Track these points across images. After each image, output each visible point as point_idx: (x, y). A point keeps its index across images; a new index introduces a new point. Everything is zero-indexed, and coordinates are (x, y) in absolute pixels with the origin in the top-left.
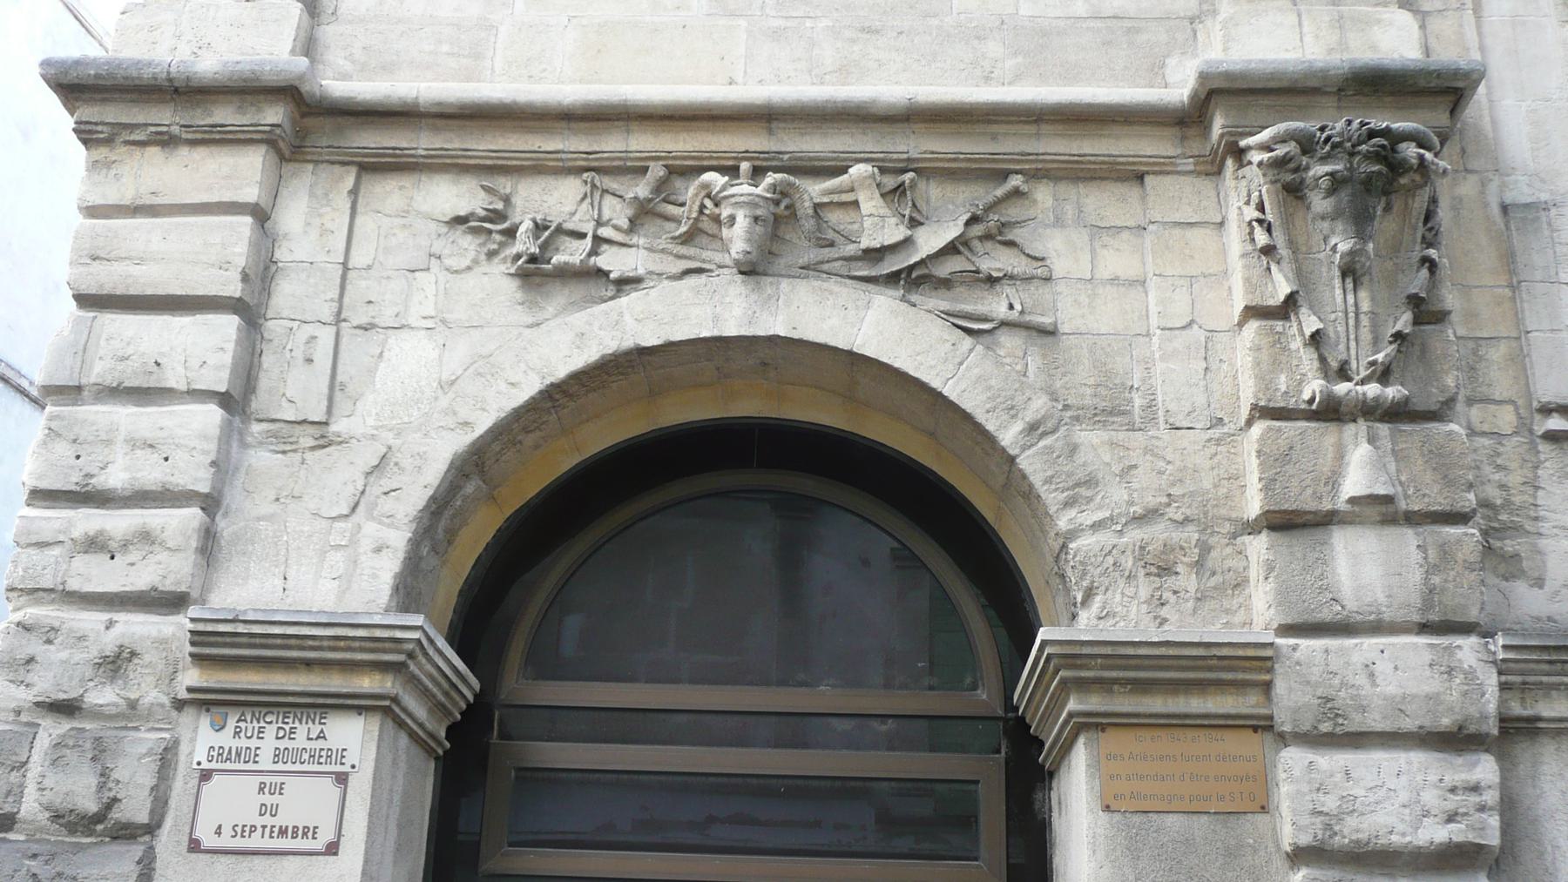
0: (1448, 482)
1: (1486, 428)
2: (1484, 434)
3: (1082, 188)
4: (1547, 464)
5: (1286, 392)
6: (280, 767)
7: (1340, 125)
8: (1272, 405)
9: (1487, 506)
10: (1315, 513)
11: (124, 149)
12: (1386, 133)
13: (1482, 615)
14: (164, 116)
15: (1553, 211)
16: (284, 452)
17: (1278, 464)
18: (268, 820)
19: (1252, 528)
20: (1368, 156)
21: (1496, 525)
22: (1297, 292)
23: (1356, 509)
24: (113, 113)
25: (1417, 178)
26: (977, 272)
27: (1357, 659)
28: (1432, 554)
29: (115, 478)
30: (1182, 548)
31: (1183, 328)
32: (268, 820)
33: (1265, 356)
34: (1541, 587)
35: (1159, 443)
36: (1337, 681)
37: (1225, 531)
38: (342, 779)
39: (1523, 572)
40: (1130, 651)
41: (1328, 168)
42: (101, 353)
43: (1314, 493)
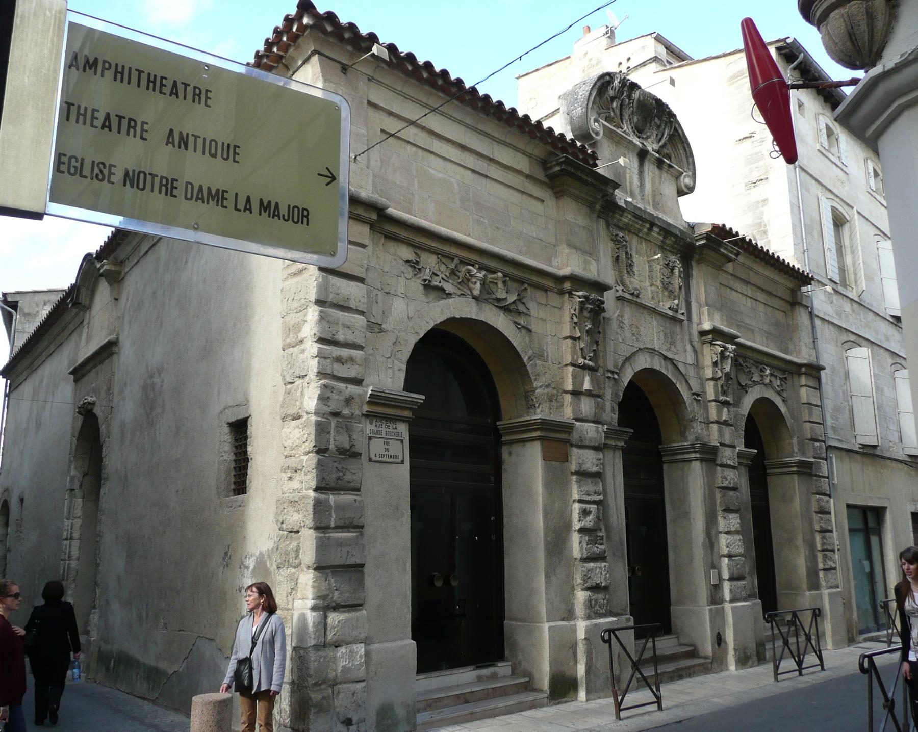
6: (387, 437)
18: (387, 453)
29: (340, 337)
32: (387, 453)
38: (402, 441)
40: (552, 422)
41: (590, 307)
42: (331, 290)
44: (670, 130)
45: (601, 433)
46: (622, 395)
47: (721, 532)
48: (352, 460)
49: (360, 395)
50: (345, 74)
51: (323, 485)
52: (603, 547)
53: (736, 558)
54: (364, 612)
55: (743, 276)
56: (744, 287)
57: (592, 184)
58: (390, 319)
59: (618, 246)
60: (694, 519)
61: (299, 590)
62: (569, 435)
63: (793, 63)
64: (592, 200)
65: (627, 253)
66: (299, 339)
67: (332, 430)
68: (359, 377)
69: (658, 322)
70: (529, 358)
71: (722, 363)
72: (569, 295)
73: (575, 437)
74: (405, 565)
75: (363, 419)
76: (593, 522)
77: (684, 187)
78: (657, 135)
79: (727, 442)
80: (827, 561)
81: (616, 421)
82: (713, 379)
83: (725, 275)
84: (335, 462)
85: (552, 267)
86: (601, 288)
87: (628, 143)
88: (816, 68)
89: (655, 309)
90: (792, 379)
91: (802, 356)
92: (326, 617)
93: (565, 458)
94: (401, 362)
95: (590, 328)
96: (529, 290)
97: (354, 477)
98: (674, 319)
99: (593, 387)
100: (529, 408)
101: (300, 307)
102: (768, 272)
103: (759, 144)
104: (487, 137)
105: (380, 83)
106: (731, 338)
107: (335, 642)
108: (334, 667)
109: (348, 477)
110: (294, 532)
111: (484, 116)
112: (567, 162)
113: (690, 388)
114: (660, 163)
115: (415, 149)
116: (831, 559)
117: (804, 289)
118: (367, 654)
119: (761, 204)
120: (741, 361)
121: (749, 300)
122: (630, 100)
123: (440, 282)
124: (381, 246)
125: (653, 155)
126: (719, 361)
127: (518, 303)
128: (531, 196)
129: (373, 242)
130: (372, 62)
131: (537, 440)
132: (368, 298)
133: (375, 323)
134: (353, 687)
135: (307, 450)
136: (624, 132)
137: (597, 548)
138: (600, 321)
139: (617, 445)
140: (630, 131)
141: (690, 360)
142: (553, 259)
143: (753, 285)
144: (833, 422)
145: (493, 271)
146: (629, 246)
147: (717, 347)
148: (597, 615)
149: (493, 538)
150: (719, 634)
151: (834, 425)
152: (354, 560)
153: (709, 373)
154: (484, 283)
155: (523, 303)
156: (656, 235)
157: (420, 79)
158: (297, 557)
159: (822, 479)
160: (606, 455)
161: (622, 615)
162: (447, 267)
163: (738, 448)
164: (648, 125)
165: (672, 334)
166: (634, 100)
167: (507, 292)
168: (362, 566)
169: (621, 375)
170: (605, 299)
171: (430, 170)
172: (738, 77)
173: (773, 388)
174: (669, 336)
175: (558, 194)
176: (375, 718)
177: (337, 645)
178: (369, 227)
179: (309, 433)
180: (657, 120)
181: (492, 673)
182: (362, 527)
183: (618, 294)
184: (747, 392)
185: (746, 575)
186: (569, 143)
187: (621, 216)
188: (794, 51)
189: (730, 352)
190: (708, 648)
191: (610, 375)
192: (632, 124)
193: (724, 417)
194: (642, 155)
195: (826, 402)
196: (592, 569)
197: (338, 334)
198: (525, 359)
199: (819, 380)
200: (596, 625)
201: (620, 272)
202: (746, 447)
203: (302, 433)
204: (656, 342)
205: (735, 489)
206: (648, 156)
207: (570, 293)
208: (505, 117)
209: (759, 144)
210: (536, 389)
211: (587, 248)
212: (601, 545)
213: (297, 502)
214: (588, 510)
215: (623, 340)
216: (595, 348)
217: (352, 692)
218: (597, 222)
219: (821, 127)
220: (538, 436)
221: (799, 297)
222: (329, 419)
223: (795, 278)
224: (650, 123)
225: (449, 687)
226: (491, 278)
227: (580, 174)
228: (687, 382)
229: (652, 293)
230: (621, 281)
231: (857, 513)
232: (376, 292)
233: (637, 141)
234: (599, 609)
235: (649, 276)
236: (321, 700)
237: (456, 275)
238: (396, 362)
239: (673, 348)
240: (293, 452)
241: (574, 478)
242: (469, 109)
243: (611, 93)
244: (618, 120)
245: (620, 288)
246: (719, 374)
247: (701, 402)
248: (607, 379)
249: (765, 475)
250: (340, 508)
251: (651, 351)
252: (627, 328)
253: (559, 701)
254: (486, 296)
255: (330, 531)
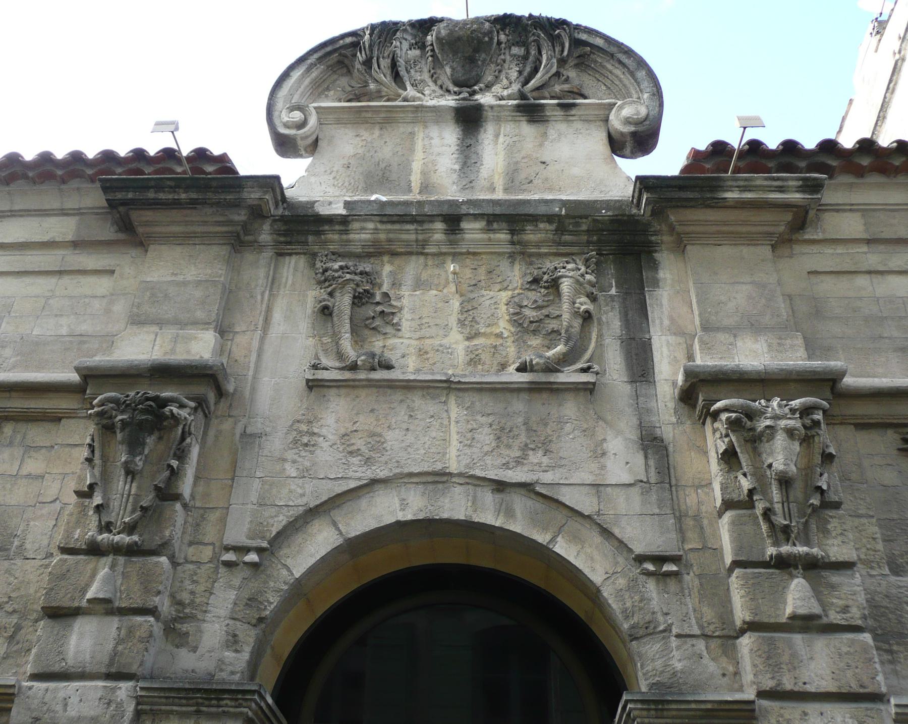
0: (147, 590)
1: (194, 559)
2: (192, 562)
3: (30, 425)
4: (221, 580)
5: (77, 539)
7: (132, 394)
8: (67, 546)
9: (180, 604)
10: (69, 608)
12: (156, 399)
13: (140, 669)
15: (264, 438)
17: (58, 580)
20: (143, 411)
21: (181, 615)
22: (96, 484)
23: (91, 606)
25: (172, 422)
27: (61, 694)
28: (123, 632)
30: (5, 628)
31: (51, 502)
33: (73, 519)
34: (195, 652)
35: (15, 567)
36: (45, 708)
37: (32, 618)
39: (188, 643)
43: (71, 597)
163: (893, 701)
166: (432, 45)
191: (651, 567)
228: (606, 533)
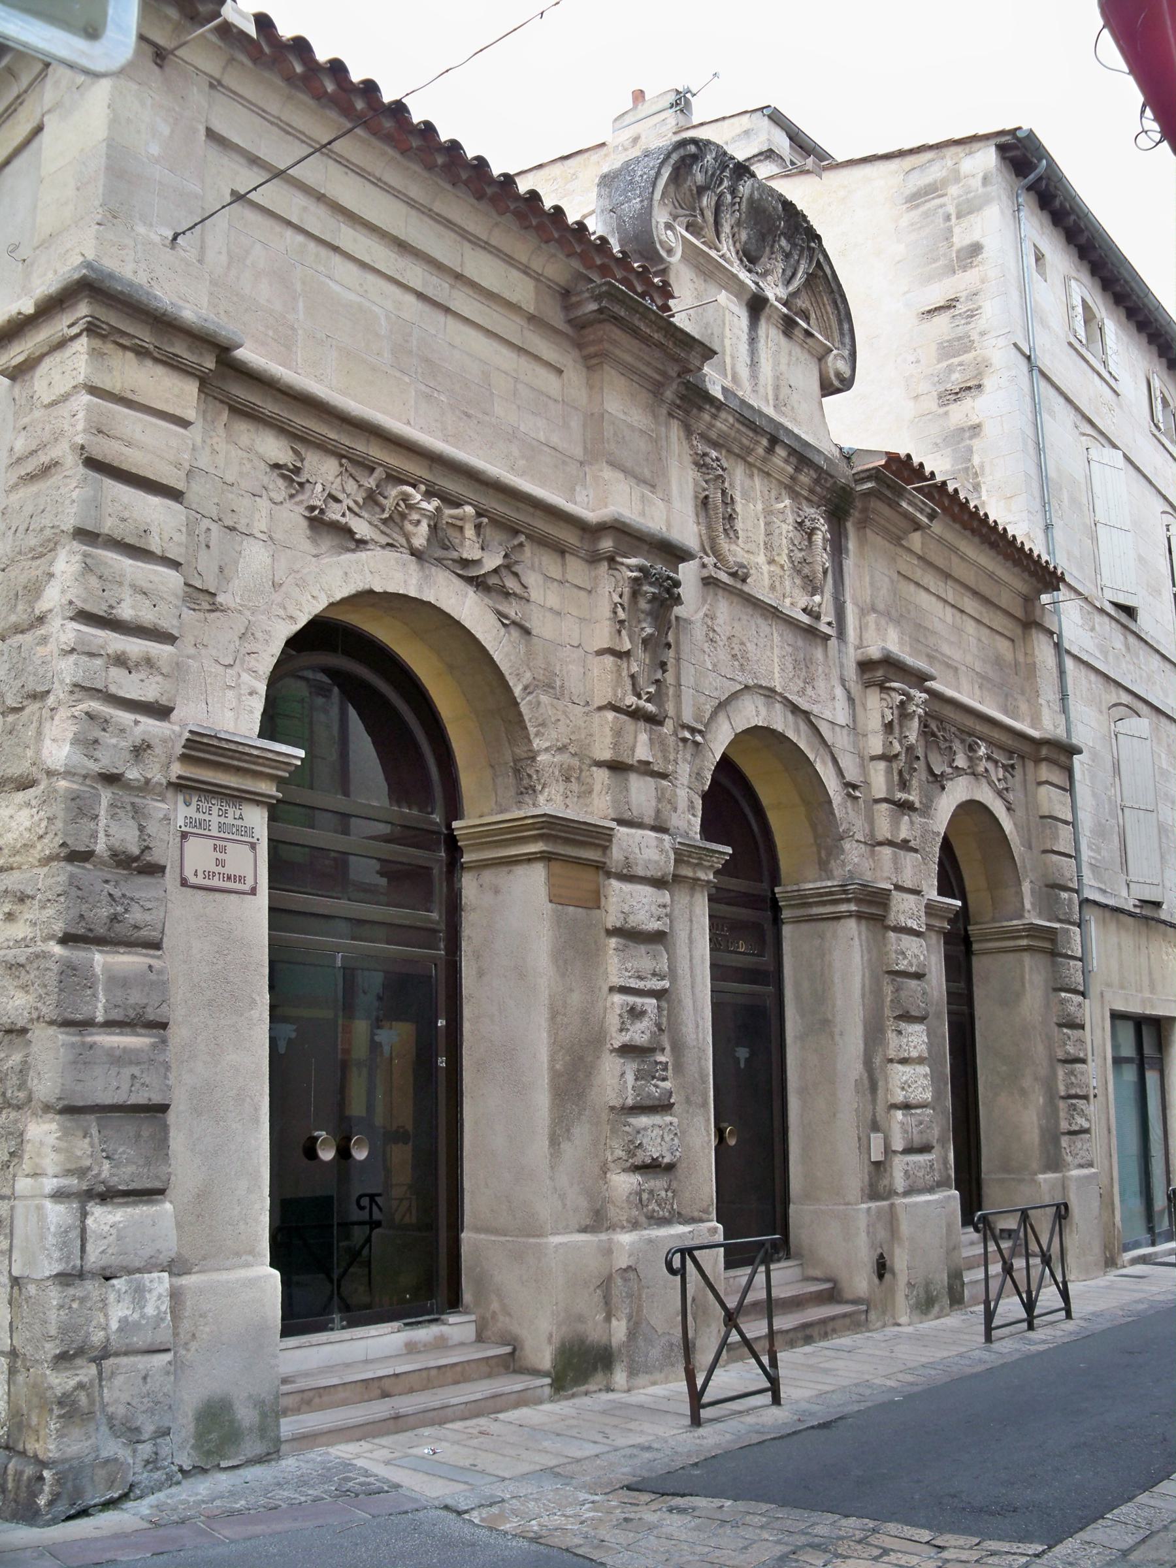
6: (222, 835)
11: (111, 346)
14: (145, 336)
16: (194, 610)
18: (220, 869)
19: (600, 764)
24: (113, 319)
26: (504, 587)
29: (126, 612)
32: (220, 869)
38: (253, 846)
41: (653, 590)
42: (110, 510)
44: (809, 266)
45: (667, 852)
46: (710, 777)
47: (891, 1061)
48: (144, 880)
49: (164, 741)
50: (160, 66)
51: (81, 931)
52: (667, 1085)
53: (919, 1111)
54: (168, 1206)
55: (940, 562)
56: (940, 583)
57: (659, 345)
58: (236, 584)
59: (707, 477)
60: (841, 1034)
61: (26, 1156)
62: (604, 854)
63: (1025, 177)
64: (658, 377)
65: (724, 492)
66: (37, 612)
67: (102, 813)
68: (164, 701)
69: (781, 635)
70: (525, 688)
71: (901, 726)
72: (609, 565)
73: (616, 854)
74: (256, 1110)
75: (170, 794)
76: (648, 1033)
77: (833, 378)
78: (784, 270)
79: (908, 884)
80: (1076, 1116)
81: (698, 829)
82: (883, 757)
83: (908, 557)
84: (107, 882)
85: (575, 504)
86: (675, 554)
87: (729, 279)
88: (1067, 190)
89: (775, 608)
90: (1024, 766)
91: (1049, 726)
92: (84, 1215)
93: (595, 901)
94: (255, 678)
95: (652, 635)
96: (528, 550)
97: (148, 917)
98: (811, 633)
99: (653, 756)
100: (522, 793)
101: (42, 545)
102: (985, 559)
103: (963, 322)
104: (453, 230)
105: (235, 95)
106: (919, 679)
107: (104, 1269)
108: (102, 1320)
109: (136, 915)
110: (17, 1031)
111: (448, 187)
112: (613, 295)
113: (840, 773)
114: (788, 326)
115: (300, 238)
116: (1082, 1114)
117: (1045, 598)
118: (175, 1295)
119: (967, 434)
120: (933, 726)
121: (949, 610)
122: (734, 198)
123: (343, 515)
124: (221, 431)
125: (776, 308)
126: (896, 721)
127: (504, 572)
128: (537, 358)
129: (205, 419)
130: (220, 47)
131: (536, 859)
132: (189, 535)
133: (201, 590)
134: (142, 1362)
135: (47, 852)
136: (722, 256)
137: (656, 1086)
138: (670, 622)
139: (699, 879)
140: (733, 257)
141: (842, 717)
142: (578, 488)
143: (956, 581)
144: (1092, 854)
145: (454, 502)
146: (727, 479)
147: (893, 694)
148: (653, 1221)
149: (442, 1062)
150: (881, 1256)
151: (1093, 862)
152: (146, 1095)
153: (876, 745)
154: (435, 525)
155: (516, 575)
156: (782, 464)
157: (320, 96)
158: (22, 1086)
159: (1072, 963)
160: (676, 898)
161: (701, 1221)
162: (360, 486)
164: (768, 249)
165: (808, 662)
167: (483, 549)
168: (164, 1108)
169: (708, 737)
170: (680, 577)
171: (331, 284)
172: (926, 194)
173: (991, 783)
174: (802, 666)
175: (592, 361)
176: (191, 1427)
177: (108, 1275)
178: (197, 384)
179: (49, 814)
180: (783, 242)
181: (435, 1338)
182: (164, 1026)
183: (705, 573)
184: (943, 788)
185: (935, 1144)
186: (617, 259)
187: (714, 417)
188: (1029, 155)
189: (917, 706)
190: (861, 1282)
191: (687, 735)
192: (738, 245)
193: (904, 833)
194: (756, 305)
195: (1081, 815)
196: (645, 1129)
197: (123, 605)
198: (517, 691)
199: (1069, 771)
200: (650, 1241)
201: (710, 527)
202: (940, 894)
203: (36, 818)
204: (777, 675)
205: (919, 976)
206: (767, 310)
207: (611, 560)
208: (489, 191)
209: (963, 322)
210: (538, 753)
211: (647, 473)
212: (664, 1079)
213: (22, 966)
214: (639, 1009)
215: (715, 665)
216: (659, 676)
217: (143, 1373)
218: (667, 426)
219: (1075, 303)
220: (541, 852)
221: (1038, 612)
222: (94, 788)
223: (1033, 574)
224: (772, 247)
225: (347, 1365)
226: (452, 517)
227: (637, 322)
228: (835, 761)
229: (771, 577)
230: (712, 548)
231: (1127, 1033)
232: (206, 523)
233: (744, 276)
234: (657, 1208)
235: (765, 544)
236: (75, 1389)
237: (377, 503)
238: (245, 677)
239: (809, 691)
240: (18, 858)
241: (613, 942)
242: (416, 167)
243: (700, 178)
244: (710, 232)
245: (710, 560)
246: (897, 747)
247: (861, 801)
248: (681, 744)
249: (969, 952)
250: (118, 982)
251: (767, 693)
252: (721, 643)
253: (575, 1390)
254: (439, 553)
255: (94, 1030)
